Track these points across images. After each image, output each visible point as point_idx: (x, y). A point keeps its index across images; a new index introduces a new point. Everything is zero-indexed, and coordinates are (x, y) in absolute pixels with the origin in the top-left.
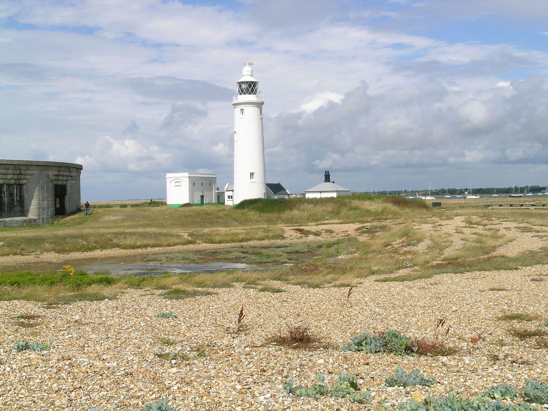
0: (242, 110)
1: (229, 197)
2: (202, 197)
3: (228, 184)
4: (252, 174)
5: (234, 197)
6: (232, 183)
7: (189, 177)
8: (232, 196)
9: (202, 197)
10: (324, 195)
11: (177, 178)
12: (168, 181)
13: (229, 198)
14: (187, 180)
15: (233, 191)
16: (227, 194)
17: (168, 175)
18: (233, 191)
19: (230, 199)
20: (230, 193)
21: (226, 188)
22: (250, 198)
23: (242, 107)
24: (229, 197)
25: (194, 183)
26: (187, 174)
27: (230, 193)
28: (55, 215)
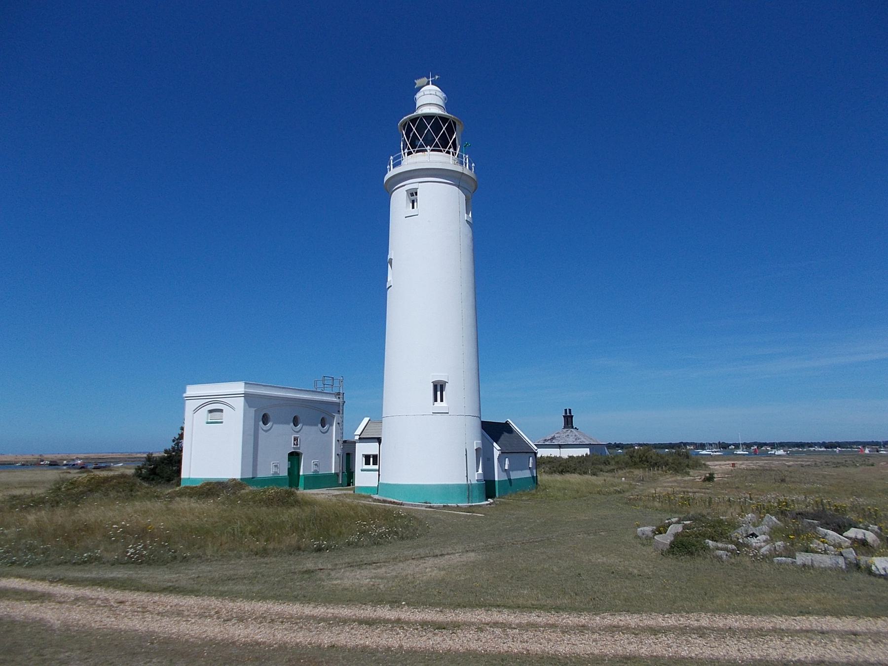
0: (413, 194)
1: (367, 458)
2: (295, 457)
3: (366, 420)
4: (439, 388)
5: (382, 460)
6: (377, 419)
7: (247, 396)
8: (375, 457)
9: (295, 457)
10: (565, 453)
11: (215, 399)
12: (190, 405)
13: (367, 463)
14: (239, 403)
15: (379, 440)
16: (362, 449)
17: (192, 390)
18: (379, 440)
19: (371, 467)
20: (371, 448)
21: (358, 432)
22: (447, 483)
23: (411, 184)
24: (367, 458)
25: (262, 414)
26: (239, 387)
27: (371, 448)
28: (565, 428)
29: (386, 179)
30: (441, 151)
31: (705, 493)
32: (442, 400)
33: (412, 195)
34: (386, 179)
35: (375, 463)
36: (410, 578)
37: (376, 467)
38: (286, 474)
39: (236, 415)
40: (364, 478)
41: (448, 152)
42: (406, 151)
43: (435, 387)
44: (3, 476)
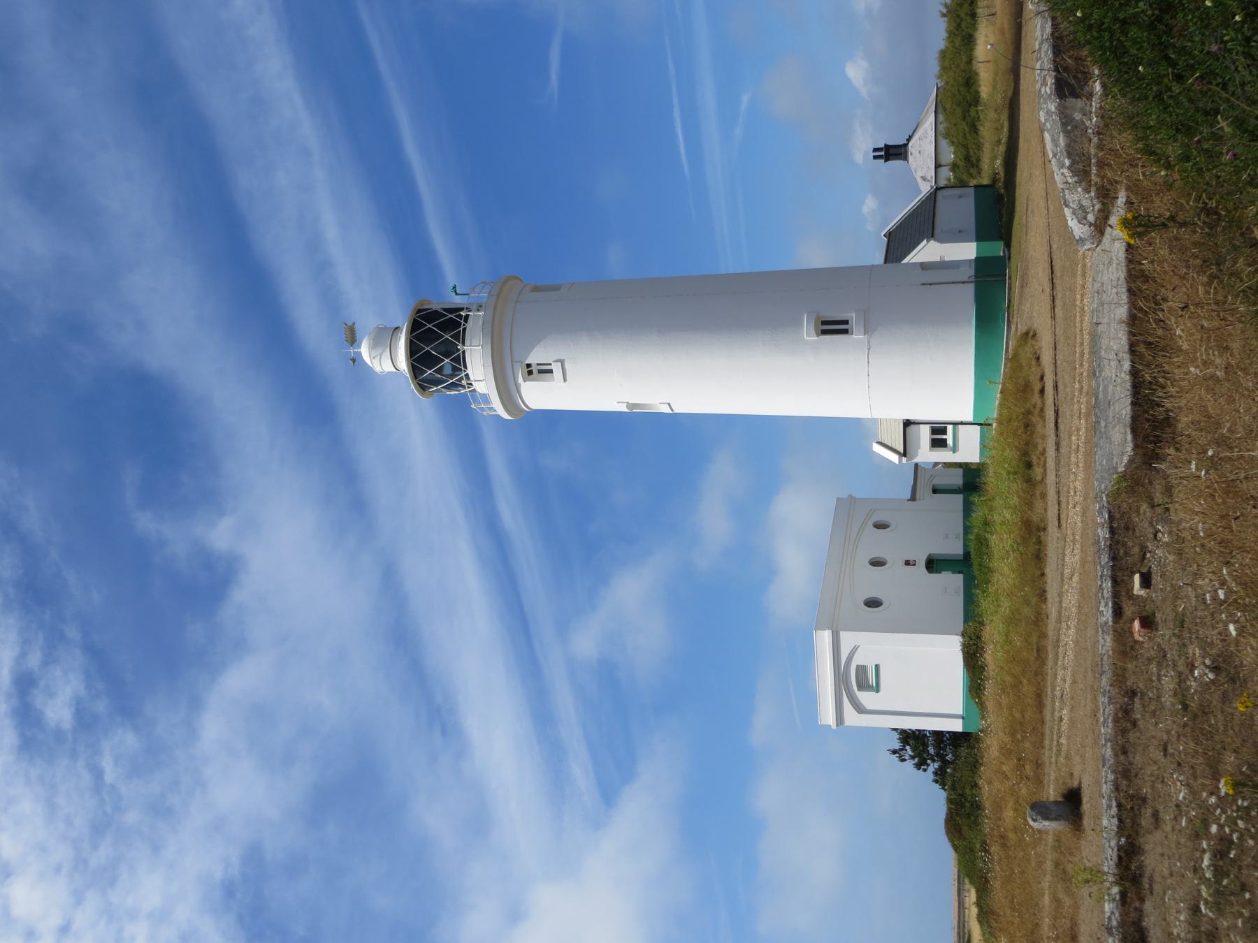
8: (935, 431)
18: (907, 424)
19: (949, 437)
21: (894, 458)
29: (506, 416)
30: (464, 330)
31: (1074, 541)
32: (846, 322)
33: (530, 373)
34: (506, 416)
35: (944, 431)
36: (1140, 145)
37: (950, 428)
38: (961, 576)
39: (869, 647)
40: (968, 448)
41: (466, 320)
42: (464, 382)
43: (824, 332)
44: (1168, 916)
